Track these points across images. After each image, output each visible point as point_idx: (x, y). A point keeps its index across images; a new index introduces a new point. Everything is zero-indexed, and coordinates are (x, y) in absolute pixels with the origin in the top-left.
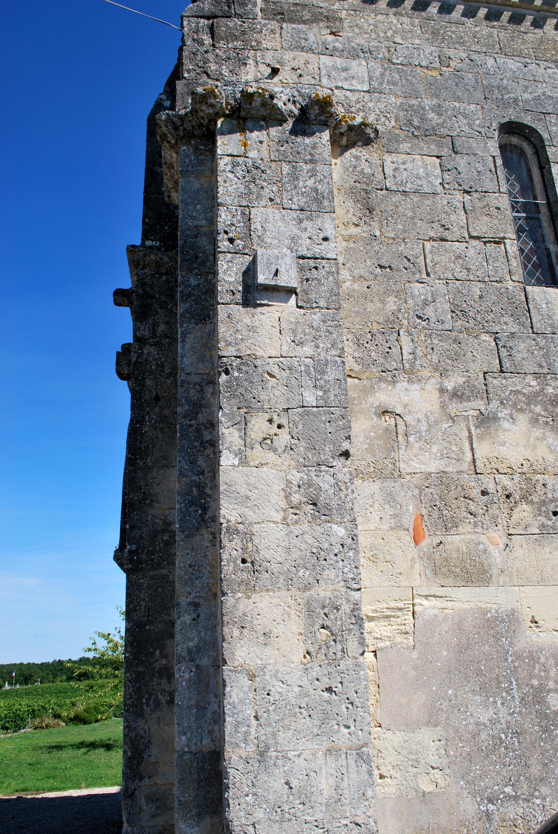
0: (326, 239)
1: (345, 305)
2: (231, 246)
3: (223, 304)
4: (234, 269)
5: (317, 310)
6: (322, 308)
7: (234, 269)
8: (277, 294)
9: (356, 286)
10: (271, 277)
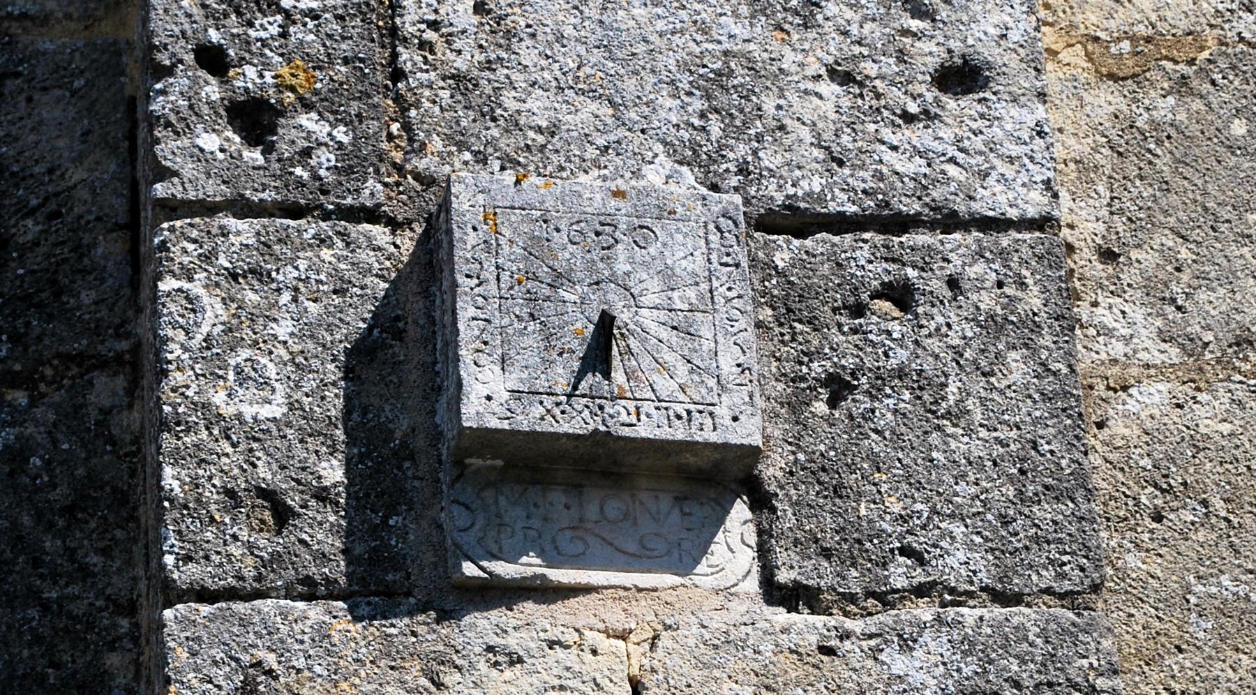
0: (962, 77)
1: (1132, 560)
2: (254, 156)
3: (204, 595)
4: (283, 329)
5: (925, 611)
6: (960, 598)
7: (283, 329)
8: (614, 507)
9: (1211, 415)
10: (561, 375)
